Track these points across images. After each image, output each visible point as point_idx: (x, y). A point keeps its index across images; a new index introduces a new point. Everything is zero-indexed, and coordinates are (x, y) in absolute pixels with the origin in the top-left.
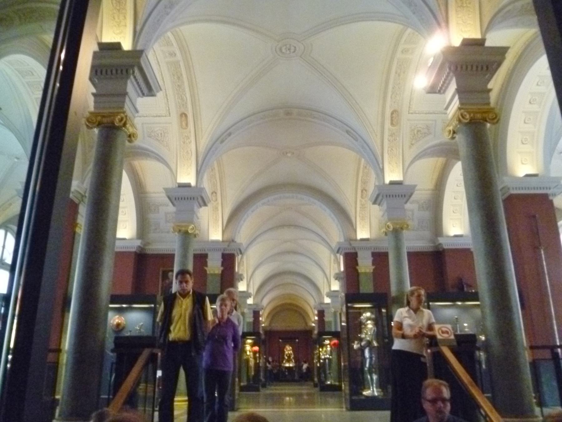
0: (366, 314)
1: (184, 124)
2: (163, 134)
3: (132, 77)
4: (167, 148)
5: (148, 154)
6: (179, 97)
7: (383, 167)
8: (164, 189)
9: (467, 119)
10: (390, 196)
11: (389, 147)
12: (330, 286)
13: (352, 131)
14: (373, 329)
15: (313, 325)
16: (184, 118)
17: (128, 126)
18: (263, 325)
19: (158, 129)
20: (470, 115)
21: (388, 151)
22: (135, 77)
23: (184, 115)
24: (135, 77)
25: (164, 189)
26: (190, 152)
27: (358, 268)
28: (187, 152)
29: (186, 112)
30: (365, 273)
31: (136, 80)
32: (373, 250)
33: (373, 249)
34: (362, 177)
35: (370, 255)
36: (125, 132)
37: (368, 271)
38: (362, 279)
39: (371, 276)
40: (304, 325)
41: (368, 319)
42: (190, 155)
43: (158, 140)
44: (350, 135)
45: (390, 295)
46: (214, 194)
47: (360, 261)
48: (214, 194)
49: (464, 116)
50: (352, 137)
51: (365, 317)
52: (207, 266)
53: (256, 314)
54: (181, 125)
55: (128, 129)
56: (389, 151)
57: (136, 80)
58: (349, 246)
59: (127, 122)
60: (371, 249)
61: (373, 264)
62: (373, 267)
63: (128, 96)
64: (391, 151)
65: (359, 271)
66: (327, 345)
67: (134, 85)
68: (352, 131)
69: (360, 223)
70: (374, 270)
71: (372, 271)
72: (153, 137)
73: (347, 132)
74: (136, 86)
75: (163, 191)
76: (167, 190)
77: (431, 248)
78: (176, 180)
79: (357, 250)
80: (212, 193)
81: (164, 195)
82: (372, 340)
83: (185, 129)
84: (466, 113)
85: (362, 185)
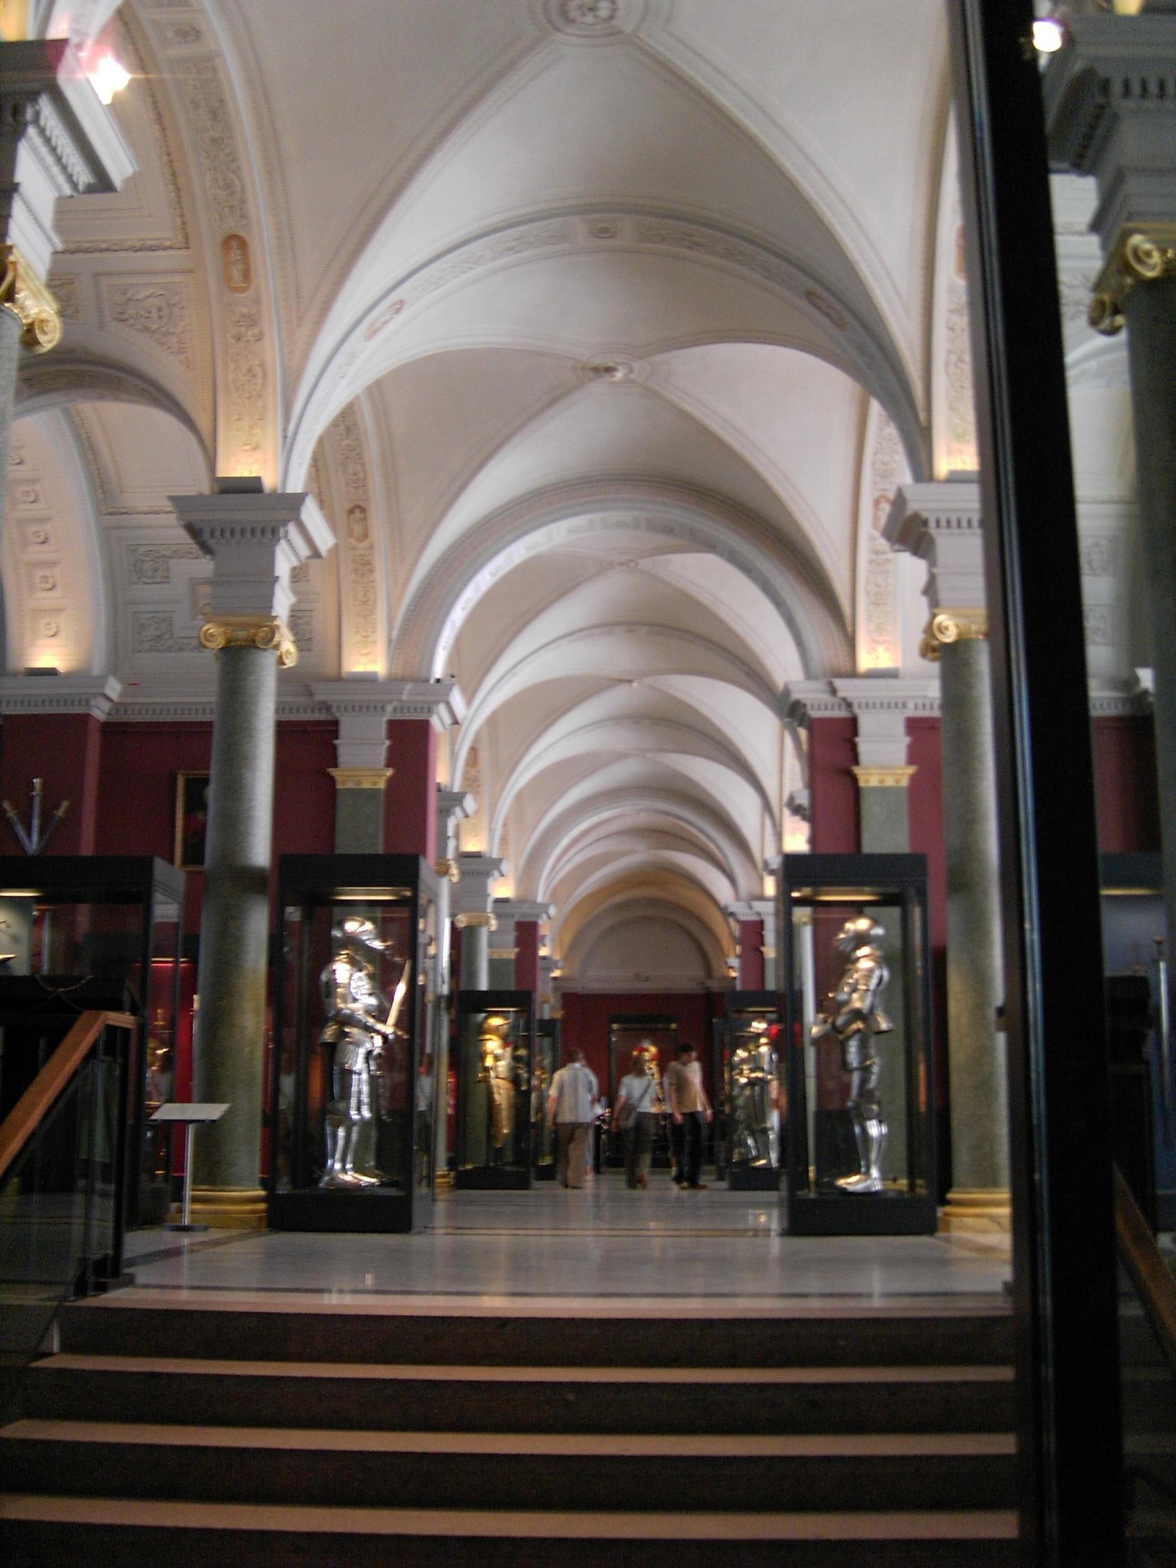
0: (854, 922)
1: (236, 273)
2: (165, 312)
3: (31, 131)
4: (182, 357)
5: (119, 378)
6: (217, 181)
7: (854, 632)
8: (172, 499)
9: (1153, 267)
10: (959, 525)
11: (950, 352)
12: (779, 836)
13: (825, 295)
14: (877, 974)
15: (733, 974)
16: (235, 254)
17: (19, 296)
18: (556, 973)
19: (148, 293)
20: (1163, 252)
21: (947, 365)
22: (42, 131)
23: (234, 244)
24: (42, 131)
25: (172, 499)
26: (258, 370)
27: (857, 770)
28: (250, 370)
29: (241, 233)
30: (882, 791)
31: (47, 141)
32: (911, 712)
33: (911, 705)
34: (875, 454)
35: (900, 728)
36: (15, 318)
37: (890, 782)
38: (872, 812)
39: (904, 798)
40: (700, 974)
41: (861, 939)
42: (260, 382)
43: (146, 329)
44: (818, 308)
45: (434, 780)
46: (358, 515)
47: (865, 747)
48: (358, 515)
49: (1143, 257)
50: (827, 315)
51: (851, 934)
52: (335, 765)
53: (527, 934)
54: (228, 279)
55: (23, 308)
56: (952, 367)
57: (47, 141)
58: (826, 698)
59: (19, 285)
60: (904, 705)
61: (911, 760)
62: (911, 770)
63: (22, 199)
64: (956, 365)
65: (862, 784)
66: (759, 1036)
67: (40, 159)
68: (825, 295)
69: (869, 618)
70: (914, 779)
71: (905, 782)
72: (131, 322)
73: (810, 295)
74: (50, 160)
75: (169, 506)
76: (181, 503)
77: (1113, 705)
78: (212, 461)
79: (857, 711)
80: (351, 512)
81: (172, 519)
82: (872, 1009)
83: (243, 290)
84: (1148, 246)
85: (875, 483)
